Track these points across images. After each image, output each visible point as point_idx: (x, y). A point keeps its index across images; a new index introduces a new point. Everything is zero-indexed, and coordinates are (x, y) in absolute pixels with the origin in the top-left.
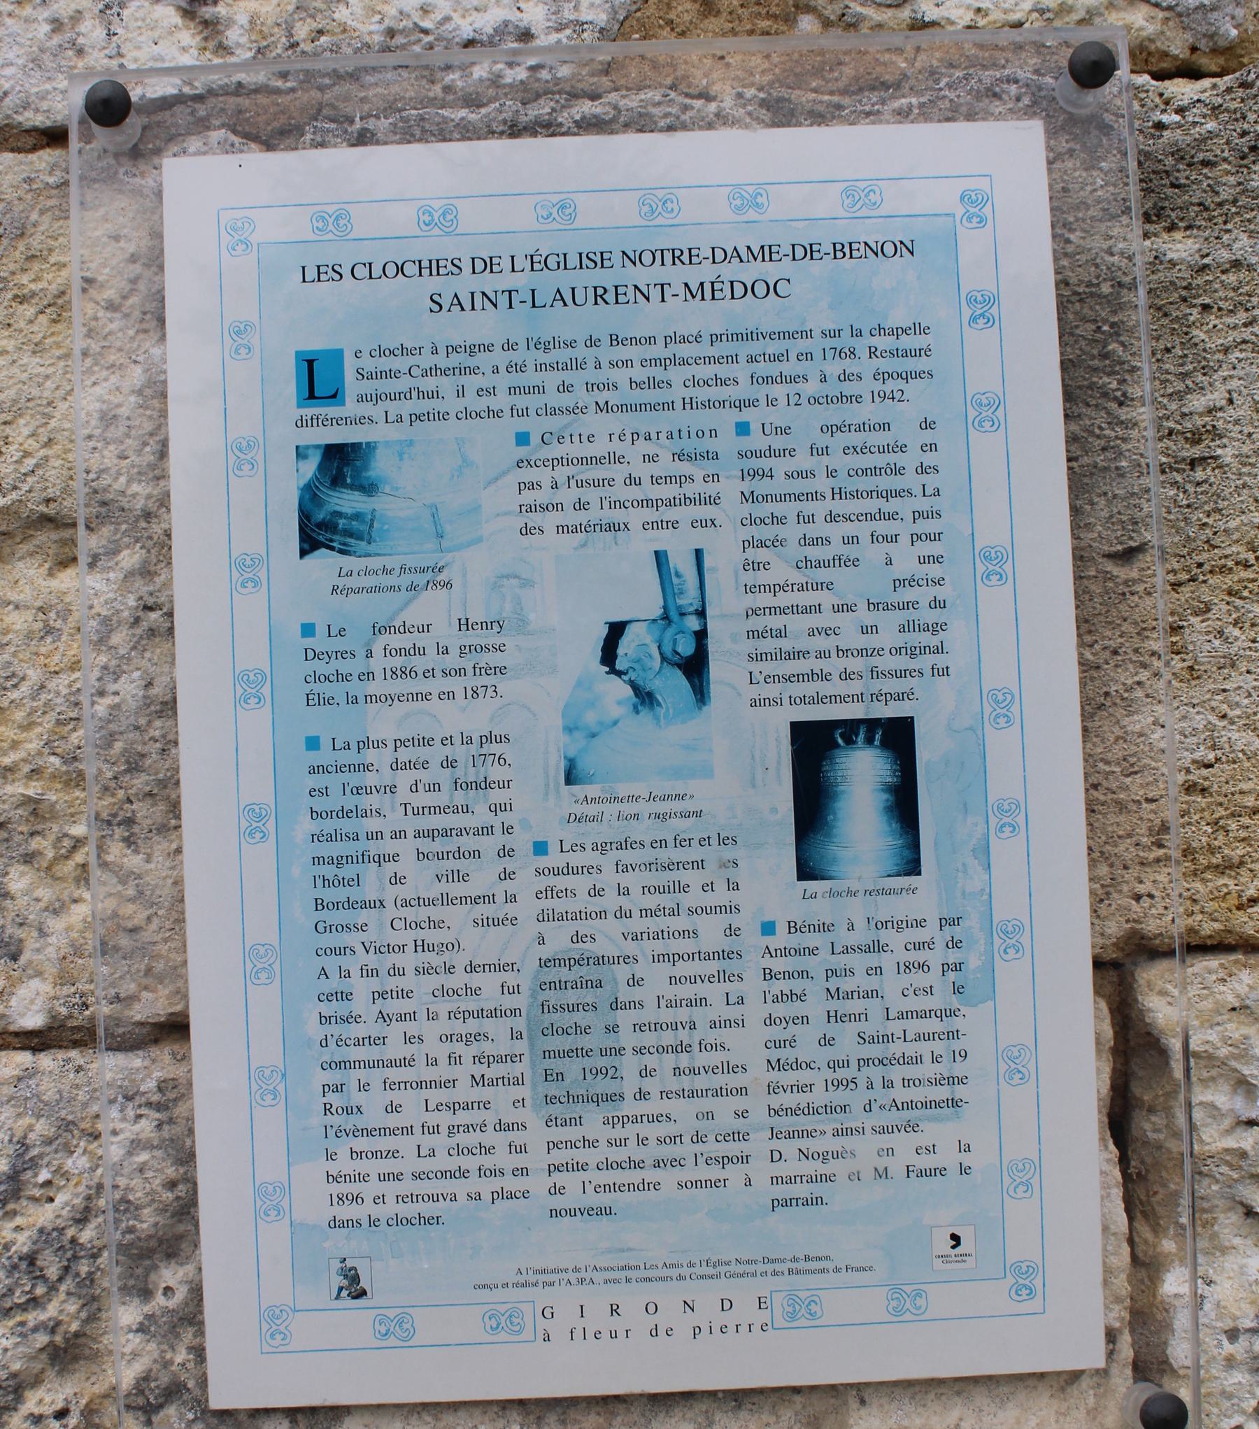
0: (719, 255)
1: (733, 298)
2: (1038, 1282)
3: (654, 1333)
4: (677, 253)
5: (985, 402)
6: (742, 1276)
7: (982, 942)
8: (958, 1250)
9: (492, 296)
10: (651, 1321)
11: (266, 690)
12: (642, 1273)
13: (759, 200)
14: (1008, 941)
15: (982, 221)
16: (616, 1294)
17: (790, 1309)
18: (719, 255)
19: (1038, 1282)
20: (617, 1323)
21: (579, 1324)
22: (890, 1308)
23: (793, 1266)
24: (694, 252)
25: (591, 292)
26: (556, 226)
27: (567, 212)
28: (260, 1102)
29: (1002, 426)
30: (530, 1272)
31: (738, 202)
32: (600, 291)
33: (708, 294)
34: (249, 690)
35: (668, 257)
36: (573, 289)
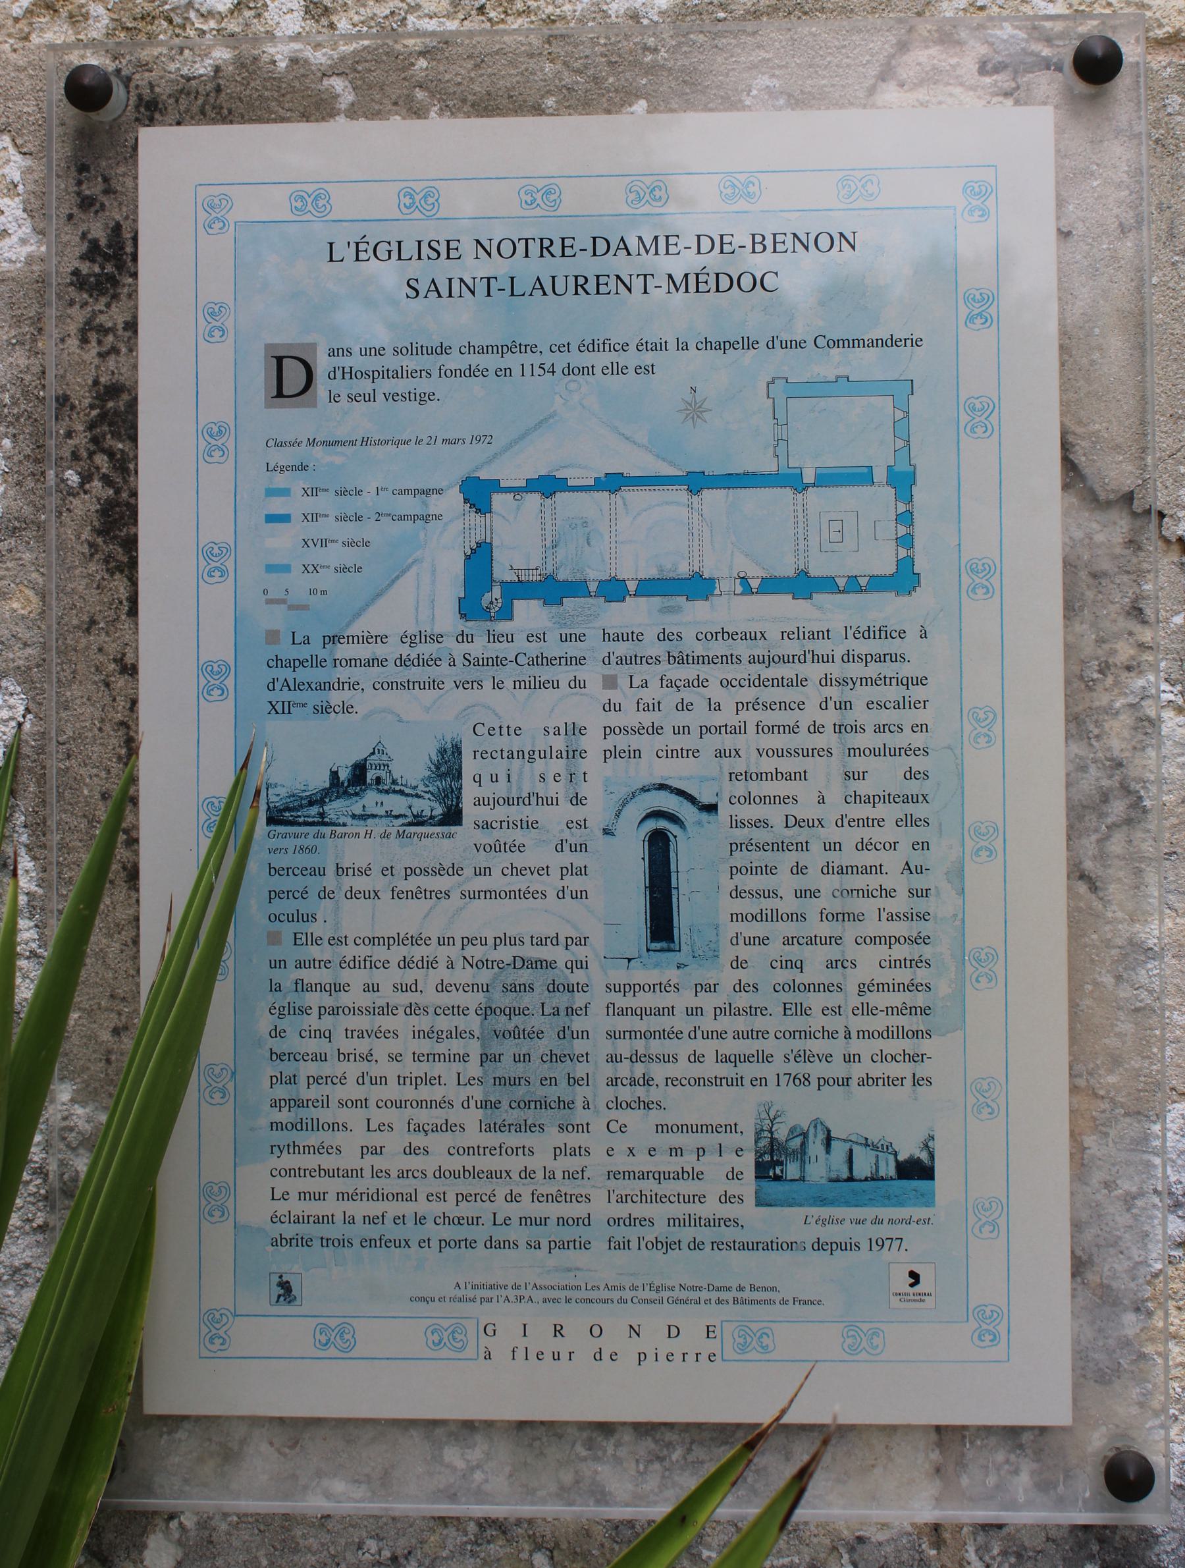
0: (601, 246)
1: (718, 290)
2: (1002, 1328)
3: (598, 1356)
4: (546, 243)
5: (978, 406)
6: (685, 1302)
7: (953, 969)
8: (917, 1289)
9: (470, 282)
10: (596, 1344)
11: (230, 682)
12: (583, 1294)
13: (751, 189)
14: (981, 969)
15: (985, 214)
16: (559, 1313)
17: (741, 1340)
18: (601, 246)
19: (1002, 1328)
20: (559, 1344)
21: (522, 1343)
22: (845, 1346)
23: (739, 1295)
24: (568, 242)
25: (571, 280)
26: (538, 212)
27: (552, 197)
28: (208, 1099)
29: (996, 433)
30: (469, 1286)
31: (729, 191)
32: (581, 281)
33: (692, 288)
34: (213, 682)
35: (534, 248)
36: (553, 278)
